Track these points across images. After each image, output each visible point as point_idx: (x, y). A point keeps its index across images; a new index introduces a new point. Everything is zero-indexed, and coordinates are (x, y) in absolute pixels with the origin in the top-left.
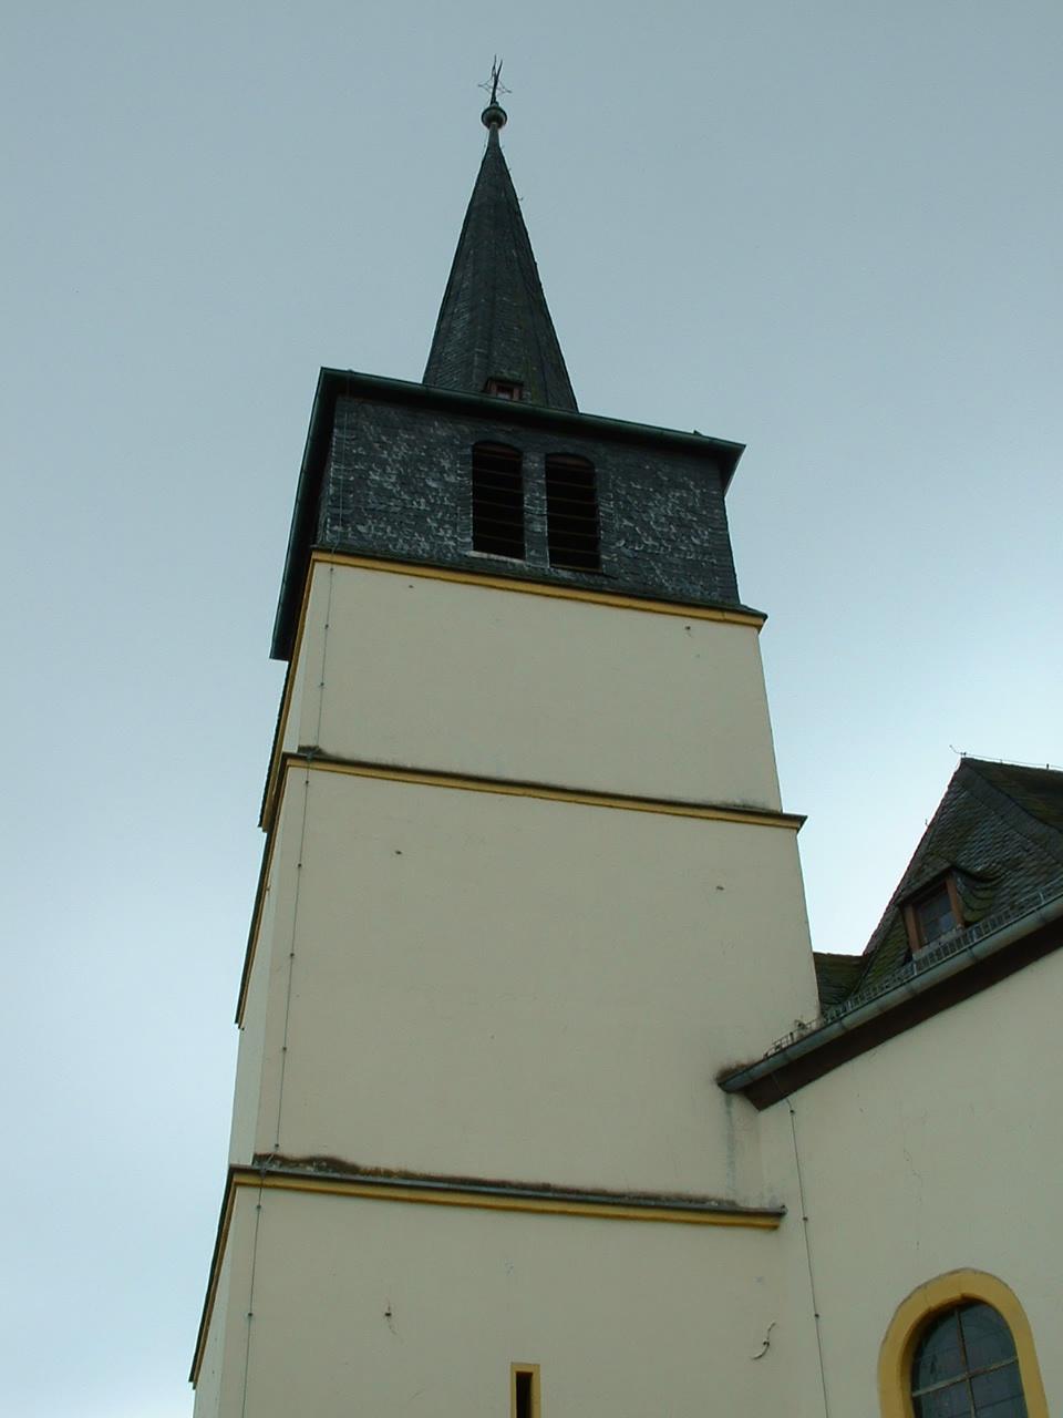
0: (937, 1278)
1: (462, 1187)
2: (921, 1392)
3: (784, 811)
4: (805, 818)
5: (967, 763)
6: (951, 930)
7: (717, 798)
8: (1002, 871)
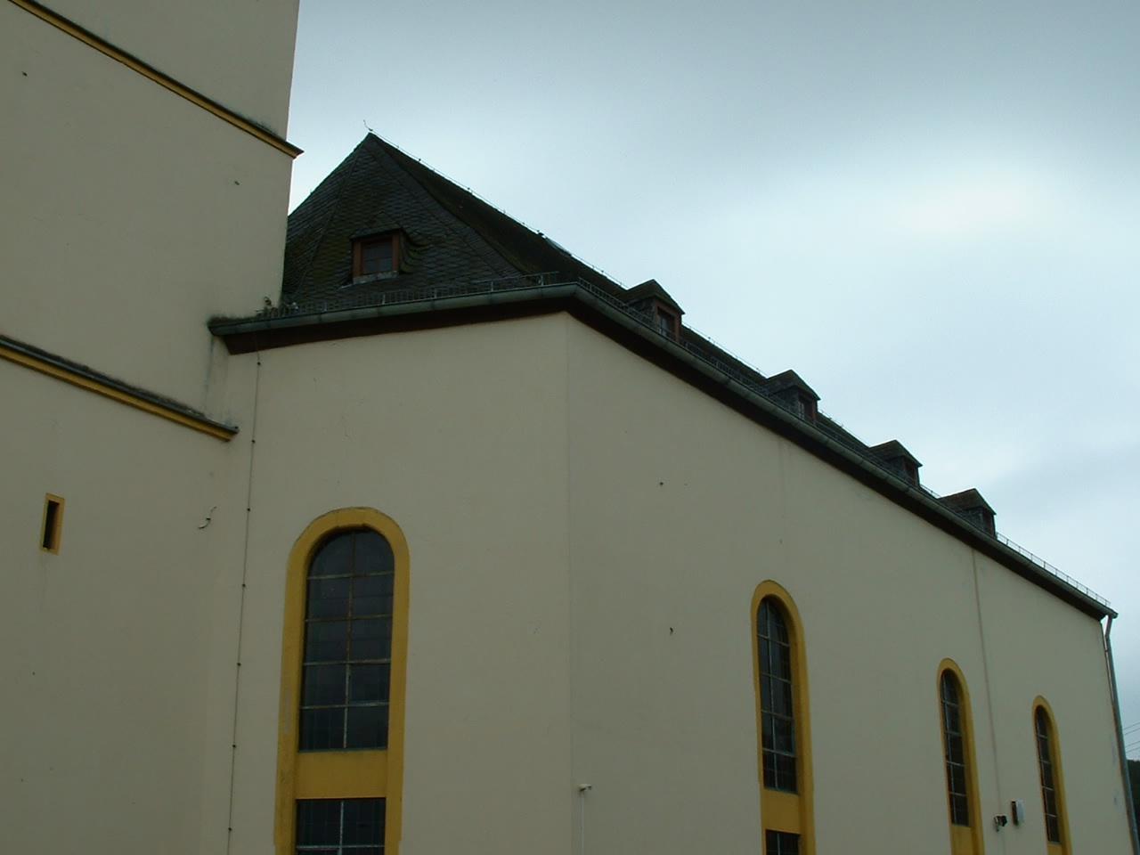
0: (349, 509)
1: (35, 355)
2: (311, 578)
3: (287, 140)
4: (302, 152)
5: (372, 138)
6: (388, 271)
7: (247, 114)
8: (454, 247)
